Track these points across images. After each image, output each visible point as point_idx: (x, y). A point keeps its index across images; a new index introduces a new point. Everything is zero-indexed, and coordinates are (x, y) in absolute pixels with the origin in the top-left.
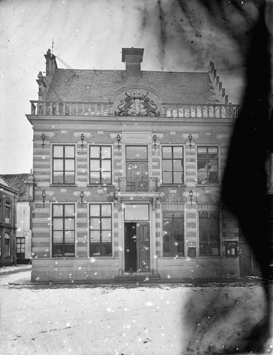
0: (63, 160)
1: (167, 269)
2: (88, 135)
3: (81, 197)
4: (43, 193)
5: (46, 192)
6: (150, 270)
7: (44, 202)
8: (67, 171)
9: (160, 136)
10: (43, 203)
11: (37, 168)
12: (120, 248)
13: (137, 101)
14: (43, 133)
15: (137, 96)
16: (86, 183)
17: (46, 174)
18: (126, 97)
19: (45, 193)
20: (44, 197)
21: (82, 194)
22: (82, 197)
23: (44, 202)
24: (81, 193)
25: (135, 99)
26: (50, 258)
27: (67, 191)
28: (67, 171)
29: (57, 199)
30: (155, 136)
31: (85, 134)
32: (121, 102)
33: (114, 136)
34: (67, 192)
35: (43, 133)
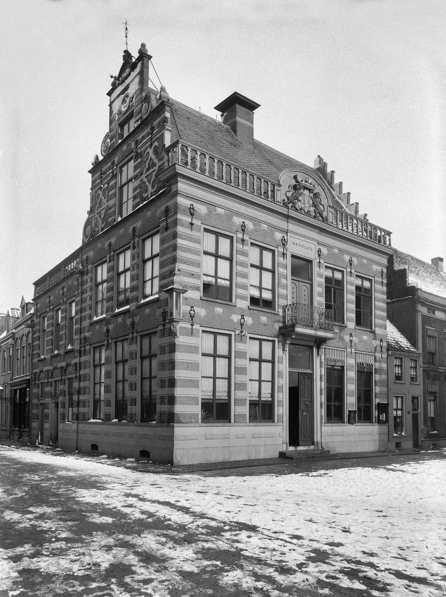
0: (219, 254)
1: (339, 449)
2: (250, 225)
3: (241, 325)
4: (191, 310)
5: (195, 308)
6: (314, 442)
7: (192, 325)
8: (208, 377)
9: (324, 251)
10: (191, 327)
11: (182, 263)
12: (282, 410)
13: (306, 192)
14: (192, 203)
15: (308, 185)
16: (246, 302)
17: (196, 277)
18: (294, 183)
19: (194, 310)
20: (192, 317)
21: (242, 321)
22: (242, 325)
23: (192, 325)
24: (242, 318)
25: (305, 188)
26: (198, 425)
27: (223, 311)
28: (208, 377)
29: (97, 509)
30: (319, 251)
31: (247, 222)
32: (289, 187)
33: (279, 236)
34: (223, 313)
35: (192, 203)
